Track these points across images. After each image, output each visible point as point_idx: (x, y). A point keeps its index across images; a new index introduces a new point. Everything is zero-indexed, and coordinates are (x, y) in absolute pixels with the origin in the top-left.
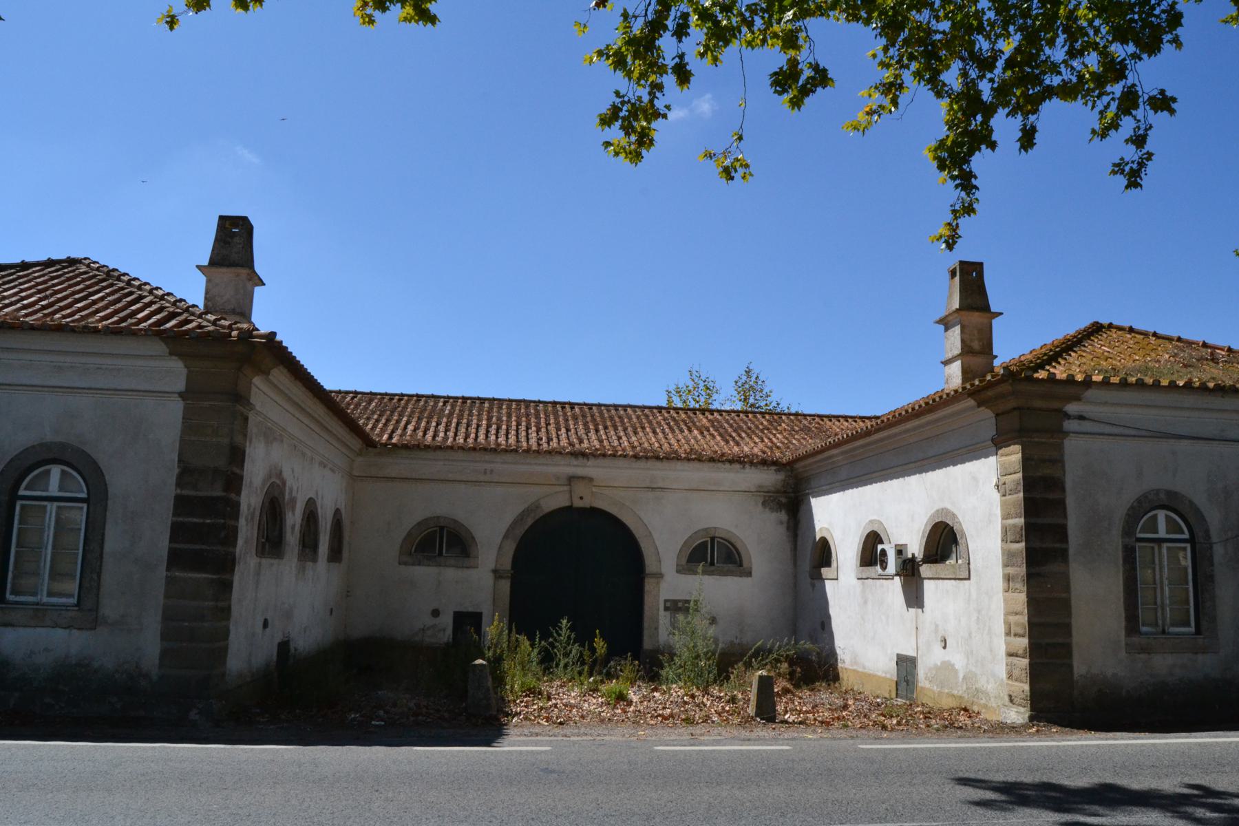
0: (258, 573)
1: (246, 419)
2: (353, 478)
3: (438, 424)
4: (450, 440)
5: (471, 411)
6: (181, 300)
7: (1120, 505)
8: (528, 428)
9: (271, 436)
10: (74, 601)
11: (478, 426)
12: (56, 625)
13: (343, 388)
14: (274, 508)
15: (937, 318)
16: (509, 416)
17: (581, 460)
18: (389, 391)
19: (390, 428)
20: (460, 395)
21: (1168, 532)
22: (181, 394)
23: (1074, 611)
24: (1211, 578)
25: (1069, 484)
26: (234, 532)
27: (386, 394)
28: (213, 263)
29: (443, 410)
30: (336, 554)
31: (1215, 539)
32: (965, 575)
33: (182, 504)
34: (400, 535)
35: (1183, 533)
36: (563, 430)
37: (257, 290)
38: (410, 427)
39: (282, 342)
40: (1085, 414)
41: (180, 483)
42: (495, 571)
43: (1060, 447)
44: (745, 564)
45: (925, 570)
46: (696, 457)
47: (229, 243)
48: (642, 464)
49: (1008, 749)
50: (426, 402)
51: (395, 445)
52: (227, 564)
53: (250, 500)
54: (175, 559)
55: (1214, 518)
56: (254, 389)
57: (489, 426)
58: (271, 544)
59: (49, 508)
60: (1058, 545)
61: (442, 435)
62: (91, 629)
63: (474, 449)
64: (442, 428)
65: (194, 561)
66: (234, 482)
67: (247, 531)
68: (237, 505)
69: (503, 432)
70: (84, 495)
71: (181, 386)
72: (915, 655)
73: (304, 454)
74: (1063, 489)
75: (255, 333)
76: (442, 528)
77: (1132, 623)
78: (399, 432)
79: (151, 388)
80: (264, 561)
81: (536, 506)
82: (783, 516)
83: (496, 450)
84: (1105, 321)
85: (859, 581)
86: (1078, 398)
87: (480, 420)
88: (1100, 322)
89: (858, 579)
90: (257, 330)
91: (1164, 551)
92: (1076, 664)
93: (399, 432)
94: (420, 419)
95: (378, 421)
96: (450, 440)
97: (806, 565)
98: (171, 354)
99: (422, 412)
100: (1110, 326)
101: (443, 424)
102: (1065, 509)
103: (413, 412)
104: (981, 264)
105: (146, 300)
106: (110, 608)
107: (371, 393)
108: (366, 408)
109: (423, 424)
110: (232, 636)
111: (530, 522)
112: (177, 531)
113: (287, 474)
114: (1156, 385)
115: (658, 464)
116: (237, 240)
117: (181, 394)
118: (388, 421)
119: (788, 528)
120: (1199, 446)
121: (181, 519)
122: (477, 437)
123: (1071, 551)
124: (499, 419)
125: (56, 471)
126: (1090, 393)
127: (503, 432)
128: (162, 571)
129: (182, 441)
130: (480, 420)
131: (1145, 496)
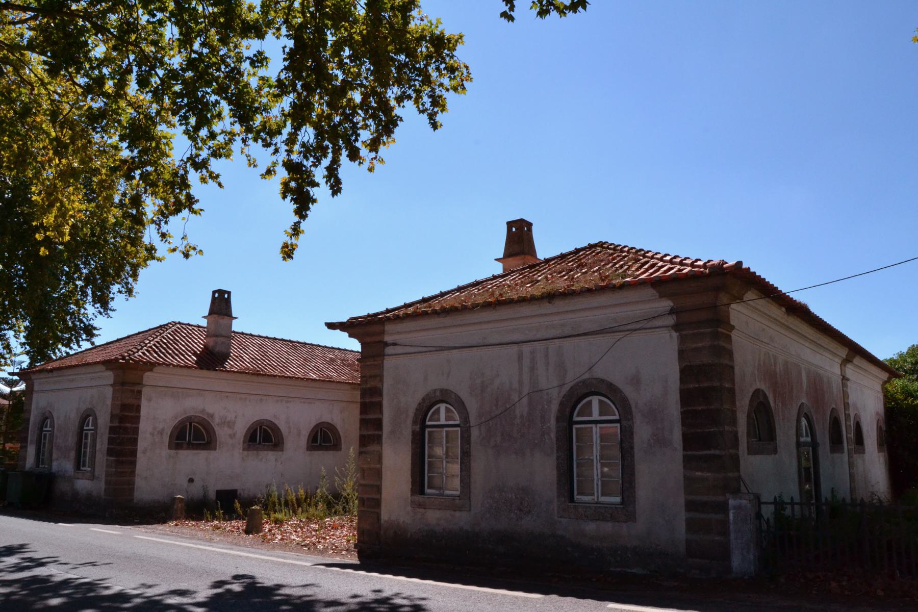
7: (411, 401)
10: (458, 493)
23: (383, 476)
28: (210, 314)
39: (749, 268)
40: (398, 342)
55: (472, 406)
60: (376, 433)
62: (91, 480)
70: (617, 417)
71: (112, 382)
75: (725, 266)
90: (726, 263)
92: (383, 513)
98: (107, 369)
120: (466, 353)
123: (384, 436)
125: (595, 400)
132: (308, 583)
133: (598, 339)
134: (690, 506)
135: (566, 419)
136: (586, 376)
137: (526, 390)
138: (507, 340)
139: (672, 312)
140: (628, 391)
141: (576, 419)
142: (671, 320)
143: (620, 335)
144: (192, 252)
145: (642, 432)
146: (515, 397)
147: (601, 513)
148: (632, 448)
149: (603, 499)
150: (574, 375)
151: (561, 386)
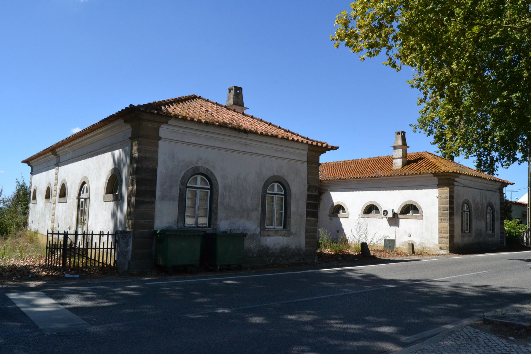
7: (461, 202)
12: (281, 235)
15: (393, 145)
21: (277, 191)
32: (422, 218)
41: (308, 190)
45: (400, 216)
47: (238, 97)
49: (434, 261)
59: (197, 192)
72: (395, 239)
79: (272, 155)
84: (198, 95)
85: (105, 202)
88: (196, 95)
89: (104, 201)
100: (200, 97)
102: (454, 203)
104: (405, 132)
106: (293, 230)
114: (472, 176)
121: (309, 202)
132: (504, 286)
146: (479, 204)
150: (268, 174)
151: (486, 203)
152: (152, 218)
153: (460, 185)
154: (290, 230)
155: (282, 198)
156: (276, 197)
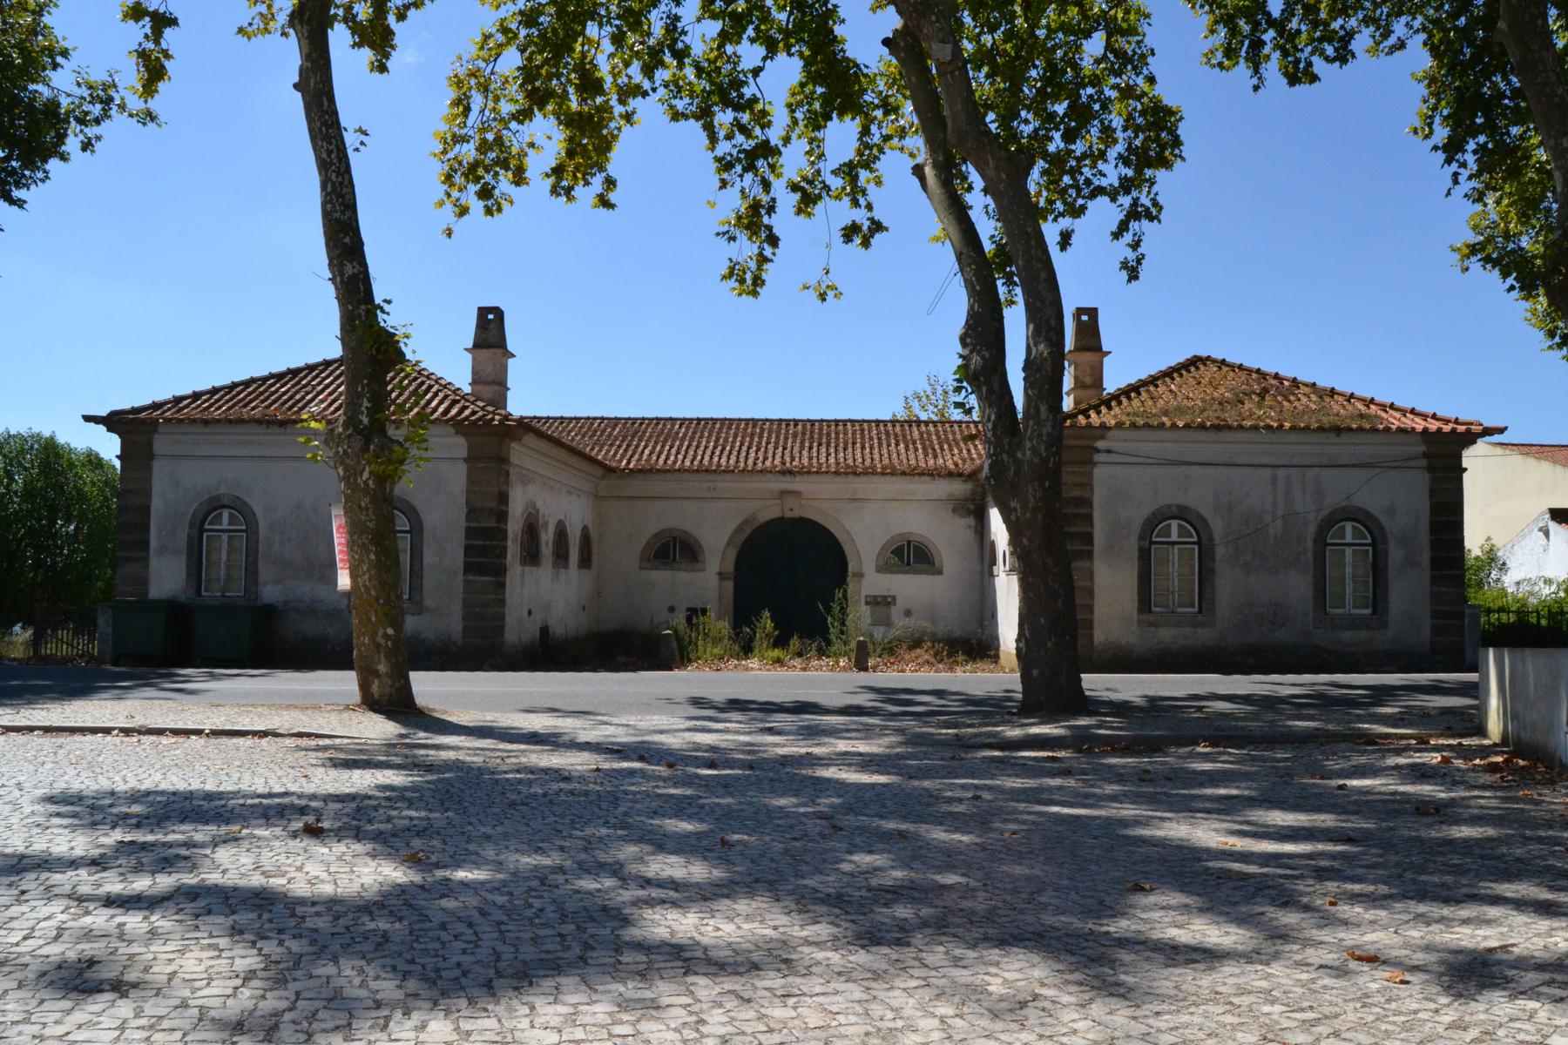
0: (522, 576)
1: (507, 473)
2: (597, 497)
3: (671, 447)
4: (679, 463)
5: (702, 433)
6: (459, 389)
7: (1137, 515)
8: (749, 448)
9: (525, 481)
11: (706, 447)
13: (592, 415)
14: (532, 530)
16: (735, 437)
17: (788, 477)
18: (633, 416)
19: (630, 453)
20: (695, 416)
22: (464, 459)
24: (1212, 571)
25: (1096, 504)
26: (505, 548)
27: (629, 419)
29: (678, 433)
30: (585, 561)
31: (1217, 540)
33: (470, 533)
34: (639, 546)
35: (1192, 536)
36: (781, 449)
37: (510, 361)
38: (647, 452)
41: (469, 517)
42: (720, 574)
43: (1090, 475)
44: (937, 564)
46: (891, 472)
48: (841, 479)
50: (664, 425)
51: (631, 470)
52: (500, 571)
53: (514, 526)
54: (469, 568)
55: (1217, 526)
56: (512, 451)
57: (715, 447)
58: (531, 556)
61: (672, 458)
63: (697, 471)
64: (673, 451)
65: (481, 569)
66: (502, 516)
67: (513, 549)
68: (505, 531)
69: (726, 453)
70: (408, 528)
71: (465, 455)
73: (552, 488)
74: (1091, 506)
76: (675, 538)
77: (1145, 603)
78: (636, 457)
80: (527, 569)
81: (753, 518)
82: (971, 521)
83: (718, 471)
86: (1102, 438)
87: (708, 442)
91: (1176, 551)
93: (636, 457)
94: (656, 443)
95: (619, 447)
96: (679, 463)
97: (986, 564)
98: (457, 433)
99: (658, 436)
101: (675, 448)
103: (651, 436)
105: (434, 389)
106: (429, 601)
107: (616, 418)
108: (610, 434)
109: (658, 448)
110: (508, 618)
111: (748, 531)
112: (468, 550)
113: (539, 505)
115: (856, 479)
116: (492, 325)
117: (464, 459)
118: (628, 446)
119: (976, 532)
120: (1209, 470)
122: (703, 458)
123: (1096, 550)
124: (726, 440)
126: (1111, 434)
127: (726, 453)
128: (460, 577)
129: (467, 491)
130: (708, 442)
131: (1159, 510)
133: (1360, 472)
134: (1435, 615)
135: (1320, 540)
136: (1344, 504)
137: (1280, 513)
138: (1256, 462)
139: (1425, 455)
140: (1384, 520)
141: (207, 527)
142: (1424, 462)
143: (1378, 470)
144: (831, 294)
145: (1395, 555)
147: (1354, 623)
148: (1386, 568)
149: (1353, 611)
150: (1333, 501)
151: (1319, 511)
152: (145, 582)
153: (1413, 463)
154: (421, 602)
155: (1367, 551)
156: (1349, 551)
